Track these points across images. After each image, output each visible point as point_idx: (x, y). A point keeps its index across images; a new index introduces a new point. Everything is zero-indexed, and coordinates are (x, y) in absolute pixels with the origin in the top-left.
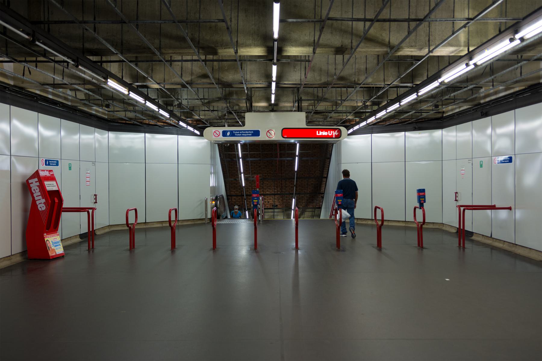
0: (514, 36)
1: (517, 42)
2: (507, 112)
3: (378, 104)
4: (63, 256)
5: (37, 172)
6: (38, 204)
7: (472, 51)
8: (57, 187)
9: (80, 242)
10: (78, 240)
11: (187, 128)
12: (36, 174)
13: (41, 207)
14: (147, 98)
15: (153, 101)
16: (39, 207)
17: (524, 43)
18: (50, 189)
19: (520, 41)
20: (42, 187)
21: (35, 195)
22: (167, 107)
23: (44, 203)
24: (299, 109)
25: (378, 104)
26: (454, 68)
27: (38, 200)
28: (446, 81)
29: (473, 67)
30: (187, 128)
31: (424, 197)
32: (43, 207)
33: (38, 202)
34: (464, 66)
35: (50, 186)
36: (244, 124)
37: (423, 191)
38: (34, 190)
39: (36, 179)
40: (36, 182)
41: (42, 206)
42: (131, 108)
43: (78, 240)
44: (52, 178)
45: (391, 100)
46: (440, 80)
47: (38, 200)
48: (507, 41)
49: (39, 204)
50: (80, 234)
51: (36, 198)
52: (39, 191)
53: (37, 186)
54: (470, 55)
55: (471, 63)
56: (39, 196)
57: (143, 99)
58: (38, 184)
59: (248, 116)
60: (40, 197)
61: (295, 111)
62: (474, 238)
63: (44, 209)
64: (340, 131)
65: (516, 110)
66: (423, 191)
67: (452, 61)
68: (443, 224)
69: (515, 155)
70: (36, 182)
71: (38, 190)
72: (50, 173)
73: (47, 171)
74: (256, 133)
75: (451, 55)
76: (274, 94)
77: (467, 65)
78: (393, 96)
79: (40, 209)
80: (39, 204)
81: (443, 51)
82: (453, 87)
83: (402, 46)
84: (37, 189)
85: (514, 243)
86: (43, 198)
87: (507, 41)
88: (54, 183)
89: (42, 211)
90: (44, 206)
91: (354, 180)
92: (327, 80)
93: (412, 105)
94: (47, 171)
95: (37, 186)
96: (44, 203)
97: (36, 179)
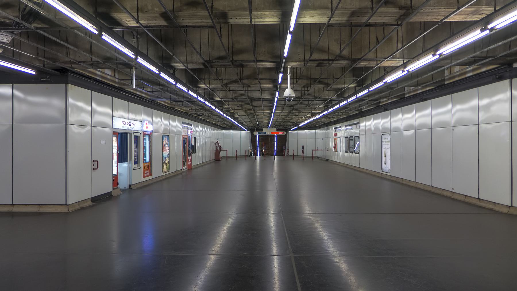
0: (404, 69)
1: (437, 57)
2: (471, 89)
3: (327, 106)
7: (405, 63)
9: (93, 206)
10: (90, 203)
11: (197, 98)
14: (199, 94)
15: (201, 96)
17: (441, 57)
19: (439, 56)
22: (193, 88)
24: (275, 128)
25: (327, 106)
26: (511, 10)
28: (388, 82)
29: (406, 72)
30: (197, 98)
34: (401, 72)
36: (262, 131)
41: (218, 149)
42: (166, 89)
43: (90, 203)
45: (333, 104)
46: (384, 81)
48: (431, 56)
50: (91, 197)
54: (404, 65)
55: (406, 70)
57: (133, 53)
59: (264, 129)
61: (274, 128)
62: (329, 161)
65: (402, 107)
67: (394, 69)
68: (416, 182)
69: (478, 124)
74: (265, 133)
75: (464, 20)
77: (403, 71)
78: (377, 77)
81: (387, 63)
82: (389, 87)
85: (401, 178)
87: (431, 56)
93: (354, 102)
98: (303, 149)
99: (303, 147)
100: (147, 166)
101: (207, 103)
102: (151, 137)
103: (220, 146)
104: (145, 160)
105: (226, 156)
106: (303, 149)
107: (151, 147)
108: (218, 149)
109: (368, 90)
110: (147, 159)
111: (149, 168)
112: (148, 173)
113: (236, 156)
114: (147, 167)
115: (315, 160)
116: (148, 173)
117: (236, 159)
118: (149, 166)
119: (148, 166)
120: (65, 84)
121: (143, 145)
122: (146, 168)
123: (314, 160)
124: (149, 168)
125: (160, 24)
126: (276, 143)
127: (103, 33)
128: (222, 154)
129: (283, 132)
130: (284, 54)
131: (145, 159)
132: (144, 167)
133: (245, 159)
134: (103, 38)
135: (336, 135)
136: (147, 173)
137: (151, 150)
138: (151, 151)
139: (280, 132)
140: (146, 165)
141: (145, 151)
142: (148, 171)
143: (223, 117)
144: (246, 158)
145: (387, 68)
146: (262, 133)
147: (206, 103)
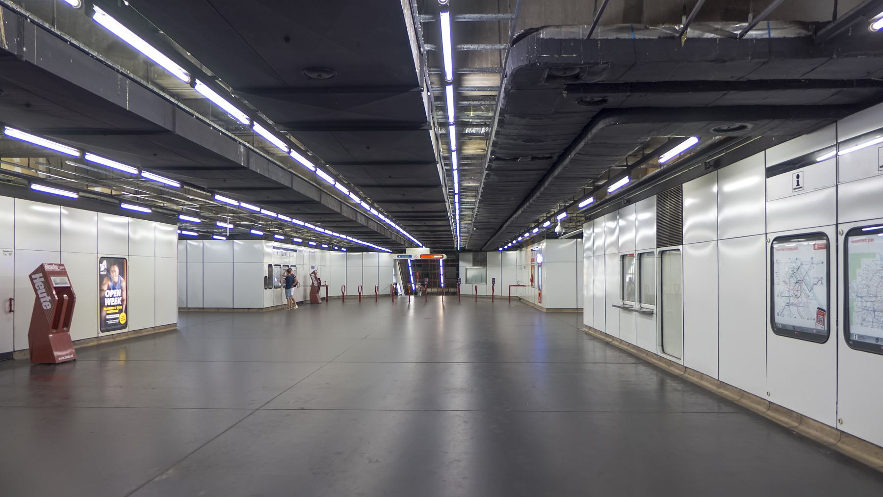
4: (74, 360)
5: (42, 266)
6: (42, 302)
8: (69, 283)
12: (41, 269)
13: (45, 306)
16: (43, 305)
18: (863, 240)
20: (47, 283)
21: (39, 292)
23: (50, 301)
27: (43, 297)
30: (292, 221)
31: (494, 281)
32: (48, 305)
33: (42, 300)
35: (57, 281)
36: (405, 253)
37: (494, 279)
38: (38, 286)
39: (41, 275)
40: (40, 277)
41: (316, 284)
44: (63, 273)
47: (43, 297)
49: (44, 302)
51: (40, 296)
52: (44, 288)
53: (42, 282)
56: (44, 292)
58: (43, 279)
60: (45, 294)
63: (49, 307)
64: (443, 256)
66: (494, 279)
70: (40, 277)
71: (43, 287)
72: (59, 268)
73: (55, 265)
76: (453, 125)
79: (45, 308)
80: (44, 302)
83: (869, 22)
84: (41, 285)
86: (48, 296)
88: (66, 278)
89: (47, 309)
90: (50, 304)
91: (849, 348)
92: (692, 34)
94: (55, 265)
95: (42, 282)
96: (50, 301)
97: (41, 275)
98: (493, 285)
99: (493, 281)
101: (339, 186)
103: (319, 279)
105: (508, 295)
106: (493, 285)
108: (316, 284)
113: (510, 296)
115: (513, 303)
117: (359, 300)
120: (28, 348)
123: (345, 304)
125: (197, 66)
127: (96, 8)
128: (322, 293)
129: (441, 255)
133: (392, 301)
135: (534, 261)
139: (436, 255)
144: (393, 299)
145: (395, 208)
146: (405, 256)
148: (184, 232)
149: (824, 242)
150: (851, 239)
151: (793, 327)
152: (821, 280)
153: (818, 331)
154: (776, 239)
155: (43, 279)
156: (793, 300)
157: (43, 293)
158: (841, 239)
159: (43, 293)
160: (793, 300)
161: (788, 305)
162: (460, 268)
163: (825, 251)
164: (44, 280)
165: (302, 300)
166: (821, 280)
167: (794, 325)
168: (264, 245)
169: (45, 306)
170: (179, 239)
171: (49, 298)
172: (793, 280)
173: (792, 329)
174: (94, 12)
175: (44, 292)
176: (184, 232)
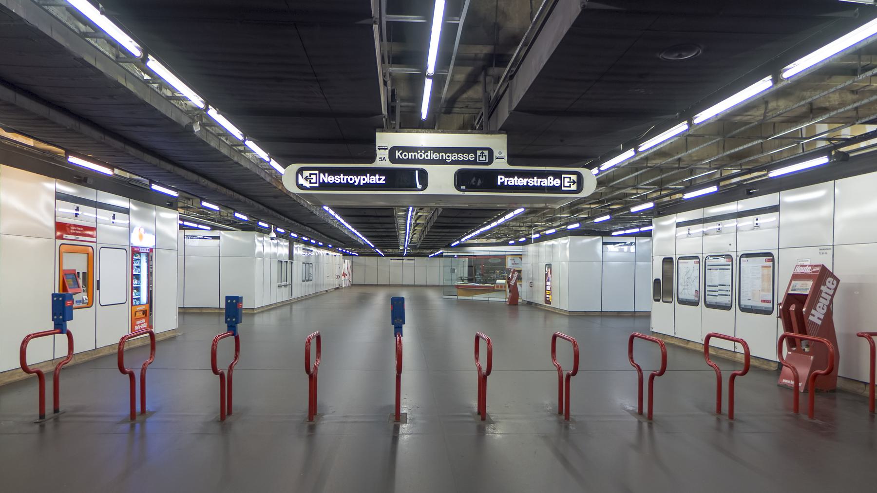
27: (828, 294)
47: (828, 294)
49: (830, 289)
52: (819, 302)
53: (816, 310)
56: (823, 298)
58: (813, 312)
60: (823, 295)
69: (779, 249)
70: (814, 316)
71: (819, 305)
80: (830, 289)
86: (822, 291)
95: (816, 310)
100: (141, 311)
102: (151, 256)
104: (138, 299)
107: (152, 275)
109: (599, 169)
110: (144, 299)
111: (146, 316)
112: (143, 323)
114: (141, 313)
116: (143, 323)
118: (146, 310)
119: (145, 312)
121: (132, 272)
122: (140, 314)
124: (146, 316)
126: (222, 111)
130: (427, 68)
131: (140, 298)
132: (133, 314)
134: (715, 185)
136: (140, 324)
137: (152, 281)
138: (152, 284)
140: (138, 309)
141: (140, 295)
142: (144, 321)
143: (358, 243)
145: (360, 230)
147: (271, 163)
148: (186, 223)
149: (698, 260)
150: (679, 261)
151: (752, 306)
152: (696, 277)
153: (695, 300)
154: (742, 256)
155: (813, 312)
156: (686, 287)
157: (824, 298)
158: (738, 259)
159: (824, 298)
160: (686, 287)
161: (684, 289)
162: (377, 257)
163: (698, 264)
164: (813, 310)
165: (654, 219)
166: (696, 277)
167: (752, 305)
168: (256, 241)
169: (833, 284)
170: (180, 229)
171: (823, 288)
172: (686, 278)
173: (715, 304)
174: (149, 60)
175: (823, 298)
176: (186, 223)
